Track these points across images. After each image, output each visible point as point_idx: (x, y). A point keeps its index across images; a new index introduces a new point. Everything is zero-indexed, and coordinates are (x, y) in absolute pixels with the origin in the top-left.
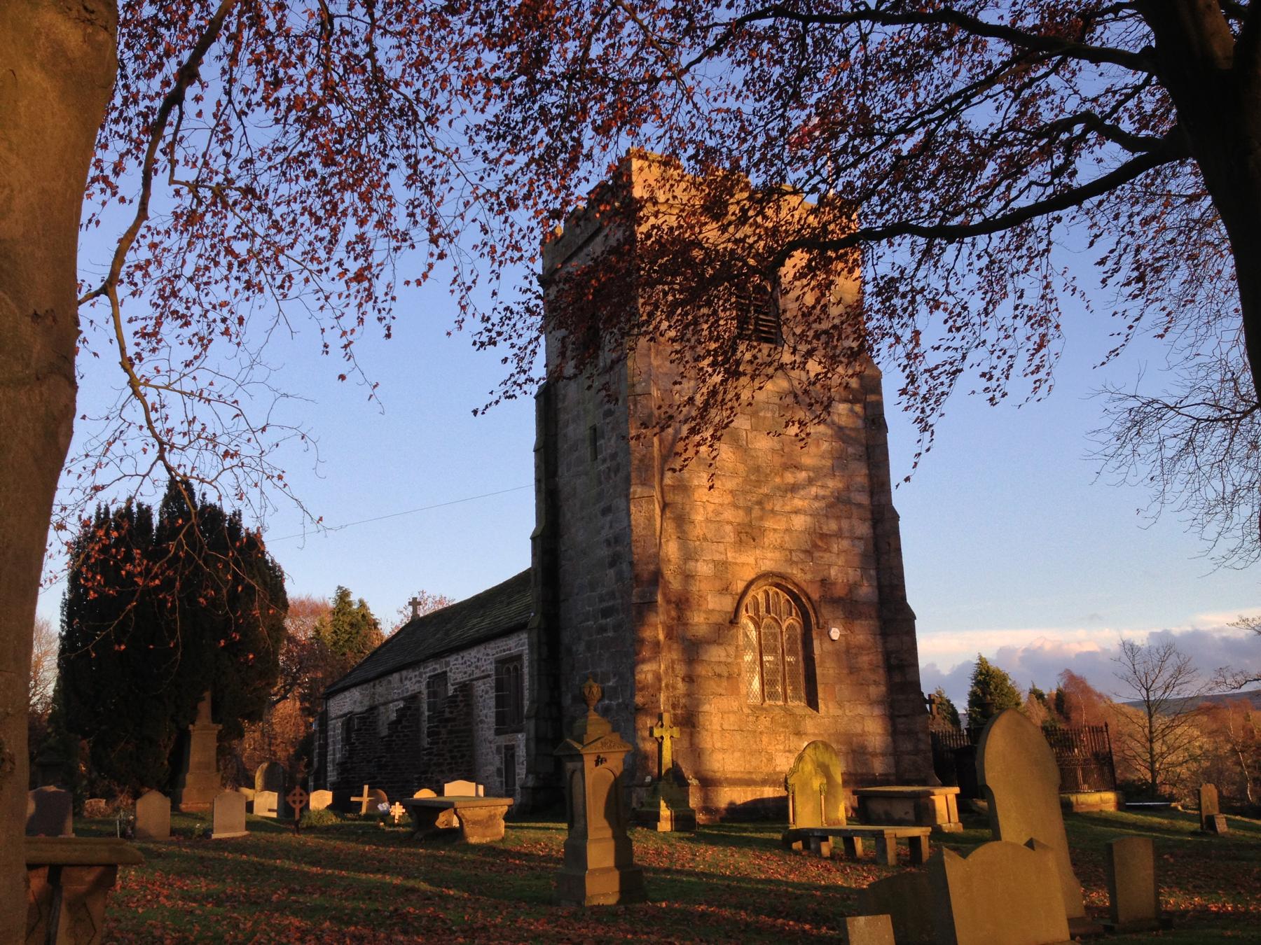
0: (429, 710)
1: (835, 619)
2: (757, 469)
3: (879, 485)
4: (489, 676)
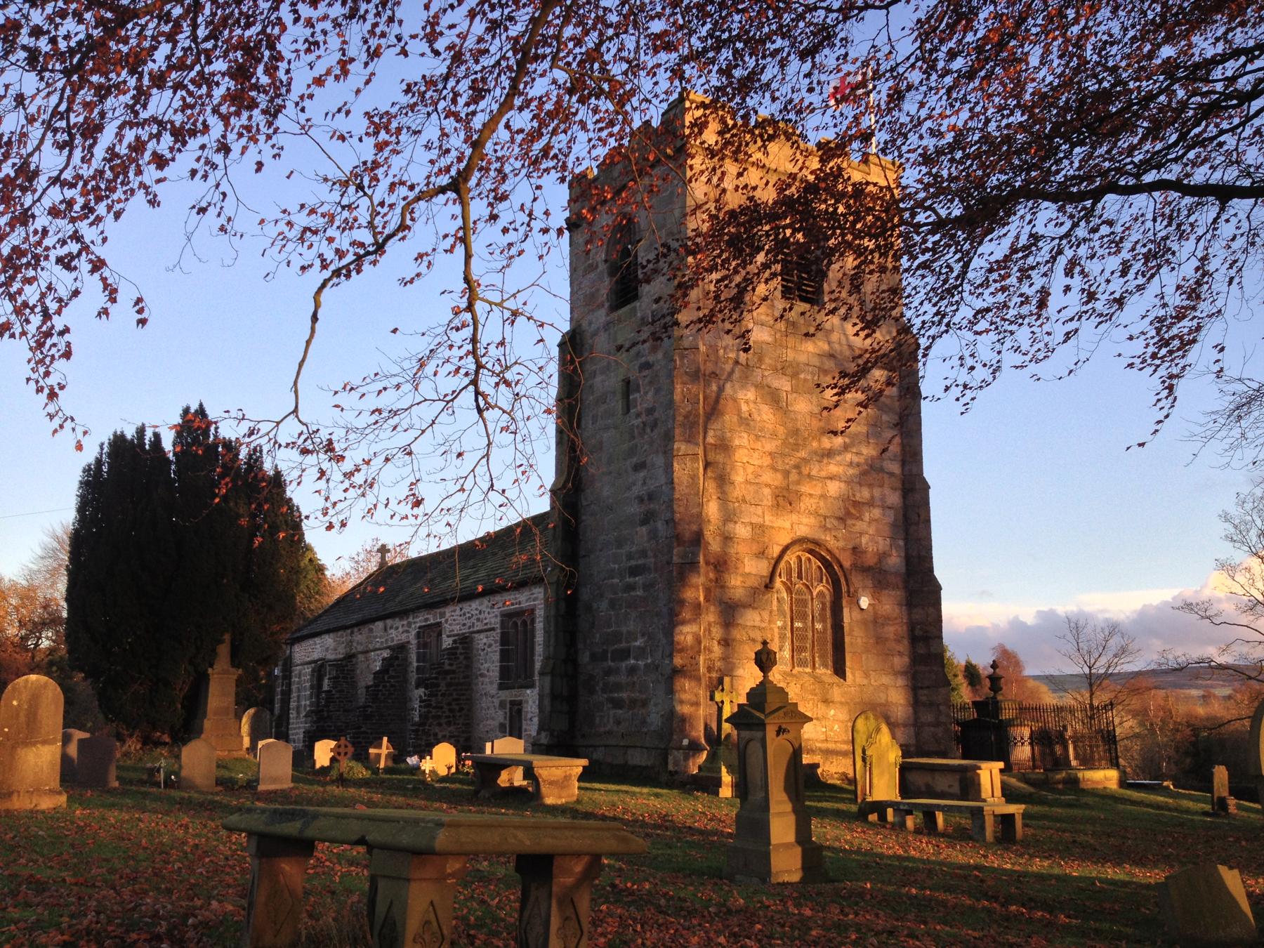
0: (418, 661)
1: (864, 588)
2: (796, 432)
3: (911, 454)
4: (493, 629)
